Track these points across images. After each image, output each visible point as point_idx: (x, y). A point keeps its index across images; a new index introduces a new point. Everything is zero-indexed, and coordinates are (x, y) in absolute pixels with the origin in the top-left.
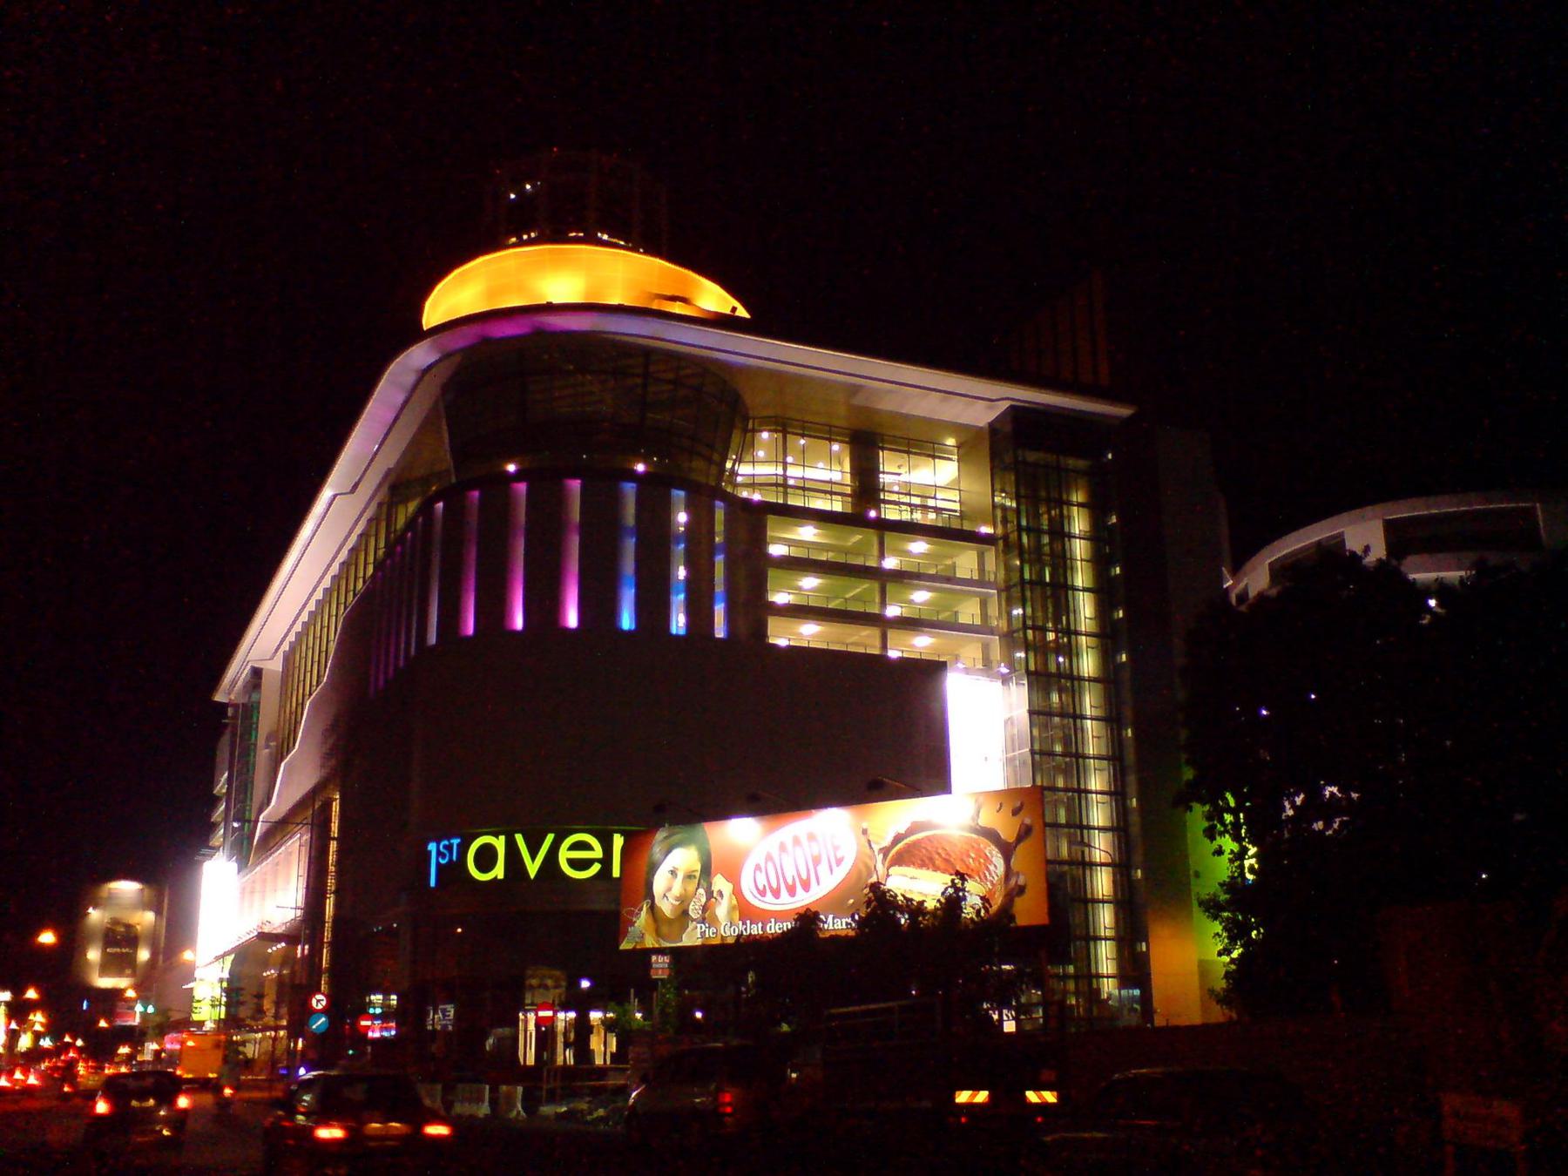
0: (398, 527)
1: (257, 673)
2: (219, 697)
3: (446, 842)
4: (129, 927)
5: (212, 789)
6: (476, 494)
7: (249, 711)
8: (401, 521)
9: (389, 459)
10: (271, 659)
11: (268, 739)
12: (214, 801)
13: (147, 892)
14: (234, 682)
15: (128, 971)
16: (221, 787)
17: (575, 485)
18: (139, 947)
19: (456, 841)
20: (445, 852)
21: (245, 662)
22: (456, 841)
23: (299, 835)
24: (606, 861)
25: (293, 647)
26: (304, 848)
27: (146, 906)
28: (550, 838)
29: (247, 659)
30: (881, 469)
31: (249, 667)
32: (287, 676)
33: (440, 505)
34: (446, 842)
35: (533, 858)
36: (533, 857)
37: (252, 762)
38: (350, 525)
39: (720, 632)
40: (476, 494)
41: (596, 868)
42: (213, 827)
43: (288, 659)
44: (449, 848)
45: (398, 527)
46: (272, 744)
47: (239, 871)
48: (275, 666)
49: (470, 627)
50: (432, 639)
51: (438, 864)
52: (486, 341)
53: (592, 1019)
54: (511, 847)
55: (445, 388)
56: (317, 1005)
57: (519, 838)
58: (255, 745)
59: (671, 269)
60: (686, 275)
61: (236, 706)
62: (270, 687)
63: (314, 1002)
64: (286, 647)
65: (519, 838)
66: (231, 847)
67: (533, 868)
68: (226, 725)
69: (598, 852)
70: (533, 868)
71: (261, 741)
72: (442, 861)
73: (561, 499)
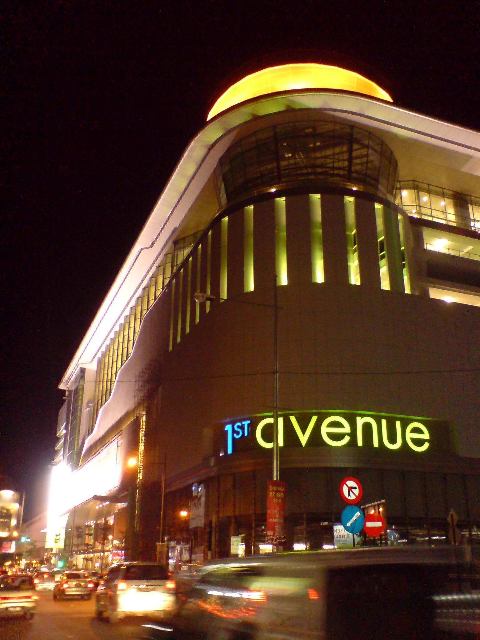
0: (179, 263)
1: (83, 371)
2: (62, 387)
3: (239, 424)
4: (8, 510)
5: (56, 433)
6: (252, 207)
7: (77, 392)
8: (180, 260)
9: (175, 222)
10: (91, 362)
11: (88, 403)
12: (57, 439)
13: (16, 495)
14: (69, 378)
15: (7, 529)
16: (62, 432)
17: (316, 197)
18: (12, 519)
19: (246, 423)
20: (240, 431)
21: (77, 364)
22: (246, 423)
23: (117, 440)
24: (353, 435)
25: (104, 355)
26: (119, 448)
27: (15, 501)
28: (314, 419)
29: (79, 363)
30: (472, 217)
31: (79, 367)
32: (101, 369)
33: (226, 219)
34: (239, 424)
35: (304, 432)
36: (304, 431)
37: (79, 415)
38: (155, 256)
39: (408, 291)
40: (252, 207)
41: (347, 439)
42: (57, 452)
43: (100, 362)
44: (242, 427)
45: (179, 263)
46: (91, 405)
47: (72, 471)
48: (92, 367)
49: (251, 286)
50: (224, 295)
51: (233, 438)
52: (256, 118)
53: (11, 574)
54: (288, 426)
55: (222, 161)
56: (349, 495)
57: (293, 419)
58: (81, 406)
59: (365, 81)
60: (372, 85)
61: (70, 392)
62: (90, 377)
63: (345, 490)
64: (99, 355)
65: (293, 419)
66: (68, 460)
67: (304, 439)
68: (64, 401)
69: (347, 429)
70: (304, 439)
71: (85, 404)
72: (236, 436)
73: (307, 206)
